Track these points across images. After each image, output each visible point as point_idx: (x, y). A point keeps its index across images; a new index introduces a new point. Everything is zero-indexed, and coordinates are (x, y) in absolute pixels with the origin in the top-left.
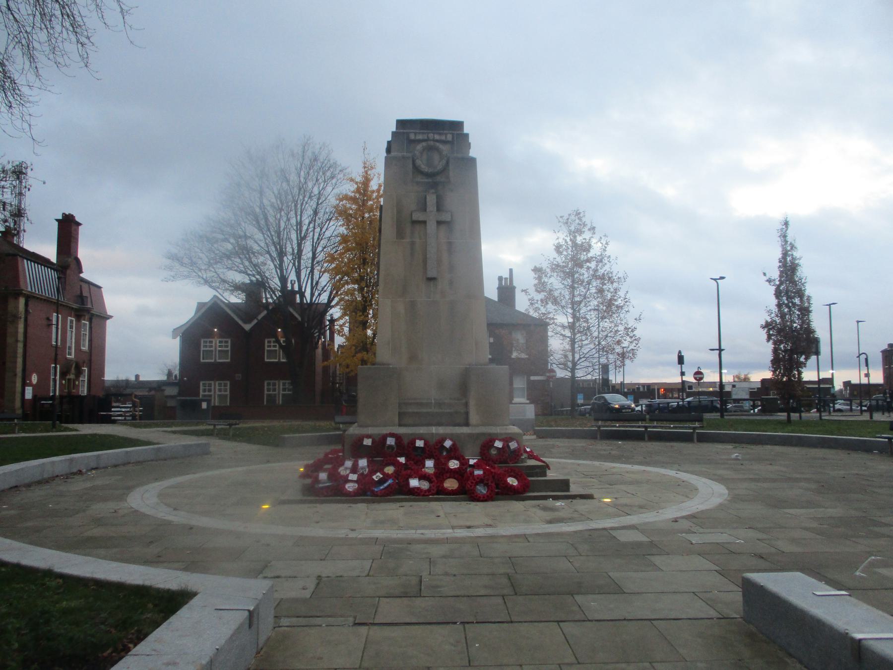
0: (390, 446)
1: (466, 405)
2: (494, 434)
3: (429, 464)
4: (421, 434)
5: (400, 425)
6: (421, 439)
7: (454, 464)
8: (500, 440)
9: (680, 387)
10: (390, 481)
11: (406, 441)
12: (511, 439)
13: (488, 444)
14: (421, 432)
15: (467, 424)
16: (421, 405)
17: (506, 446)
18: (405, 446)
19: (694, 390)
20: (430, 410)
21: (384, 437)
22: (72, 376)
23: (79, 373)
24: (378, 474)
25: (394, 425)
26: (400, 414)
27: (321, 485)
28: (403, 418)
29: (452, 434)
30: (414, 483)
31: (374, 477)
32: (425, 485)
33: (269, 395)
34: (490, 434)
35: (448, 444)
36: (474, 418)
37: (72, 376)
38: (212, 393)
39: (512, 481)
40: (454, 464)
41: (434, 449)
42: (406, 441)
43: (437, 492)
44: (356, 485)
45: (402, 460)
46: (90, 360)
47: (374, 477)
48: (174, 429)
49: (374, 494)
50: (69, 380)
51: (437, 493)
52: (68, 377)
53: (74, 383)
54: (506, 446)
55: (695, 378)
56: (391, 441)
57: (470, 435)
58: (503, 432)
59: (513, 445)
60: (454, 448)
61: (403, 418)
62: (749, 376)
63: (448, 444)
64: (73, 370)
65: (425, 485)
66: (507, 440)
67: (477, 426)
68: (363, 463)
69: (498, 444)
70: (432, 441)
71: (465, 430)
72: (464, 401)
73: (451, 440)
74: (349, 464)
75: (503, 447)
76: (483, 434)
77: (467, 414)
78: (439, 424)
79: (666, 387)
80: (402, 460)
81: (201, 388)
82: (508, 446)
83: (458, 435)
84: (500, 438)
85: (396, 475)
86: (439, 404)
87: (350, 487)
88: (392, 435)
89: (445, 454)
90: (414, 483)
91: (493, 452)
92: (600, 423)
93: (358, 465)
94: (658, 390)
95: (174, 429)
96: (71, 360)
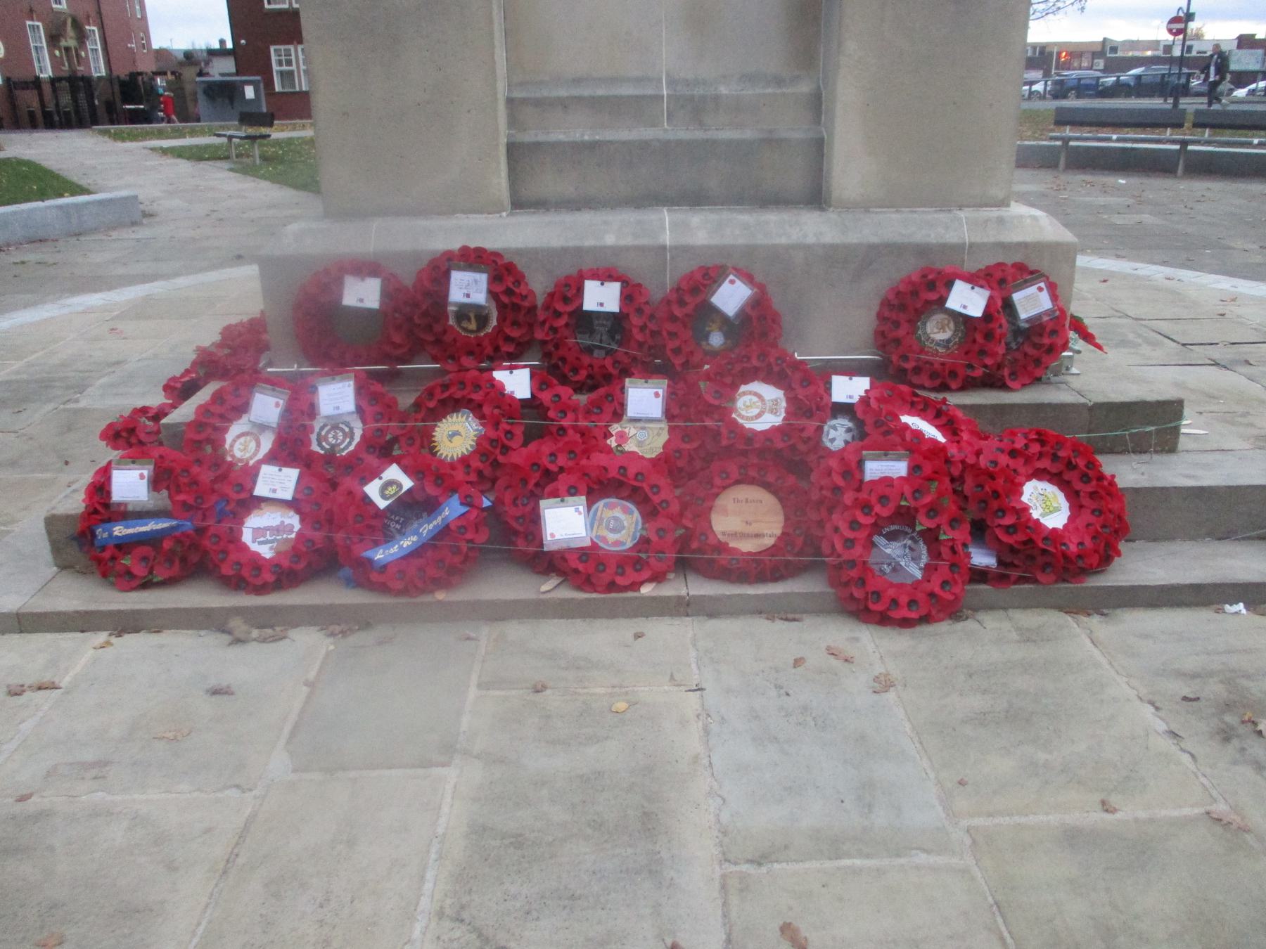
0: (465, 311)
1: (817, 105)
2: (945, 248)
3: (644, 399)
4: (601, 242)
5: (519, 204)
6: (605, 276)
7: (759, 407)
8: (973, 279)
9: (1099, 48)
10: (452, 509)
11: (539, 285)
12: (1023, 273)
13: (920, 292)
14: (610, 240)
15: (816, 197)
16: (613, 107)
17: (1001, 307)
18: (533, 315)
19: (1119, 54)
20: (647, 133)
21: (439, 271)
22: (72, 43)
23: (82, 37)
24: (393, 472)
25: (491, 208)
26: (513, 150)
27: (119, 530)
28: (528, 171)
29: (750, 251)
30: (565, 522)
31: (372, 490)
32: (619, 526)
33: (282, 73)
34: (922, 250)
35: (731, 297)
36: (851, 170)
37: (72, 43)
38: (294, 67)
39: (1046, 504)
40: (759, 407)
41: (666, 328)
42: (539, 285)
43: (678, 550)
44: (294, 521)
45: (517, 382)
46: (99, 13)
47: (372, 490)
48: (166, 143)
49: (368, 577)
50: (67, 49)
51: (684, 565)
52: (63, 43)
53: (78, 55)
54: (1001, 307)
55: (1170, 31)
56: (468, 288)
57: (835, 259)
58: (991, 236)
59: (1031, 302)
60: (760, 322)
61: (528, 171)
62: (1204, 30)
63: (731, 297)
64: (70, 32)
65: (619, 526)
66: (1001, 278)
67: (866, 206)
68: (337, 397)
69: (968, 300)
70: (659, 285)
71: (809, 229)
72: (805, 88)
73: (748, 278)
74: (267, 407)
75: (988, 315)
76: (895, 250)
77: (819, 149)
78: (696, 199)
79: (1071, 49)
80: (517, 382)
81: (274, 58)
82: (1009, 306)
83: (777, 254)
84: (971, 266)
85: (487, 465)
86: (694, 106)
87: (266, 531)
88: (474, 258)
89: (717, 340)
90: (565, 522)
91: (937, 332)
92: (1068, 131)
93: (312, 411)
94: (1059, 54)
95: (166, 143)
96: (60, 13)
